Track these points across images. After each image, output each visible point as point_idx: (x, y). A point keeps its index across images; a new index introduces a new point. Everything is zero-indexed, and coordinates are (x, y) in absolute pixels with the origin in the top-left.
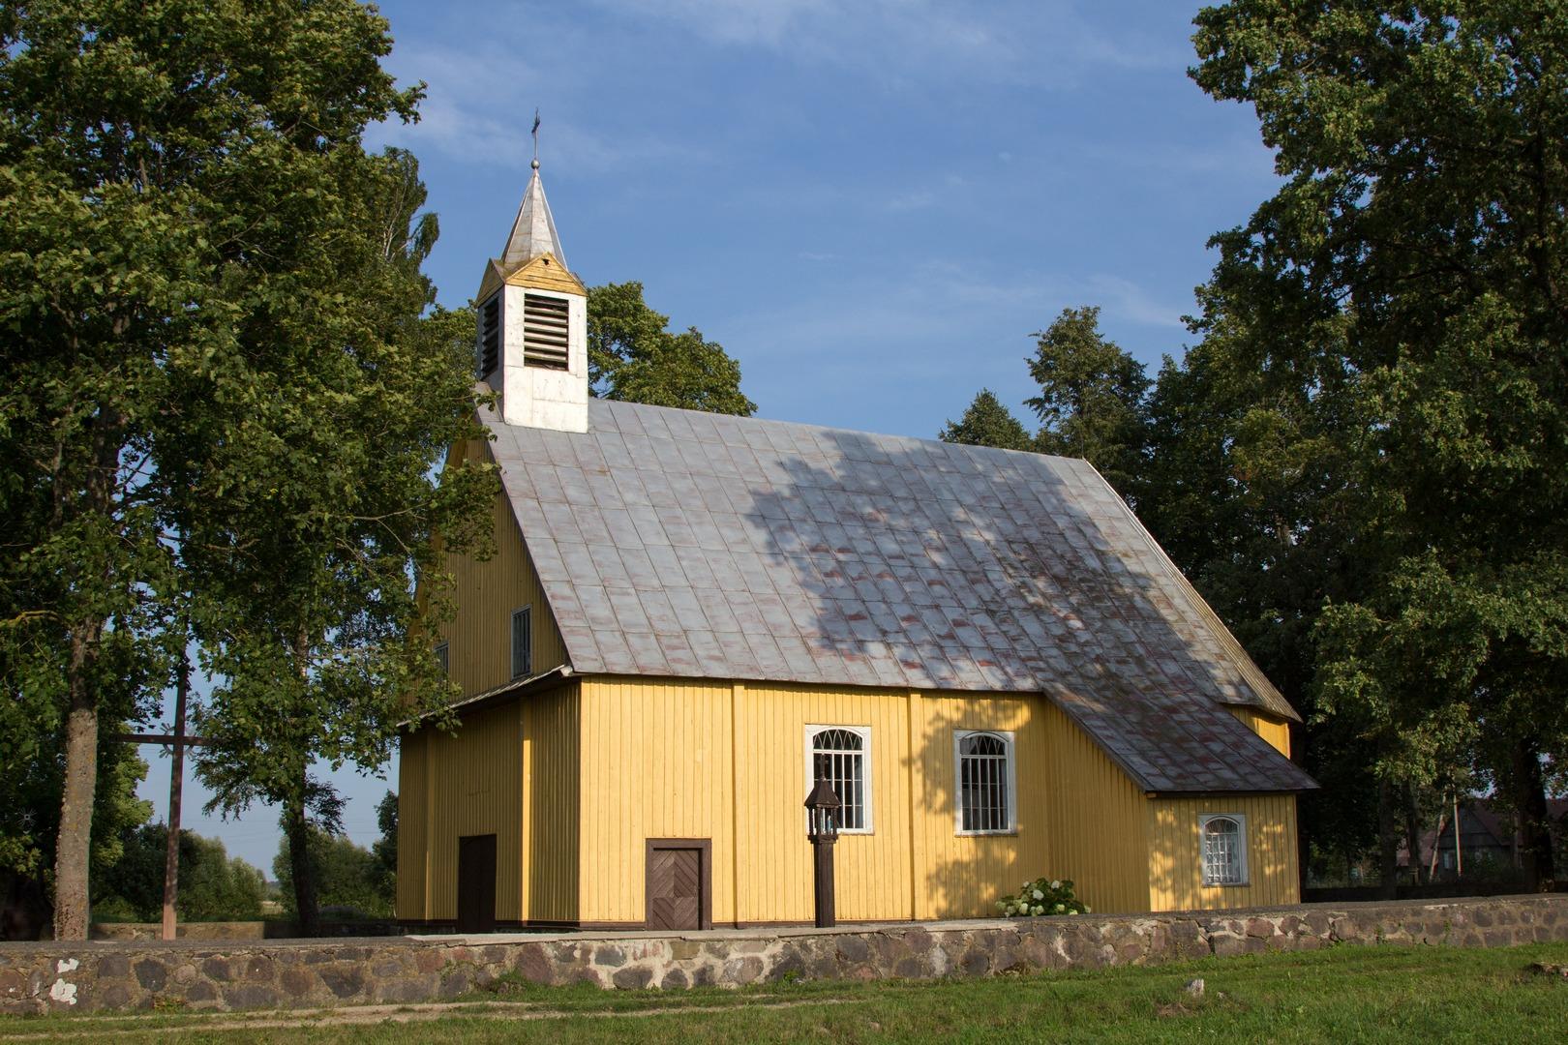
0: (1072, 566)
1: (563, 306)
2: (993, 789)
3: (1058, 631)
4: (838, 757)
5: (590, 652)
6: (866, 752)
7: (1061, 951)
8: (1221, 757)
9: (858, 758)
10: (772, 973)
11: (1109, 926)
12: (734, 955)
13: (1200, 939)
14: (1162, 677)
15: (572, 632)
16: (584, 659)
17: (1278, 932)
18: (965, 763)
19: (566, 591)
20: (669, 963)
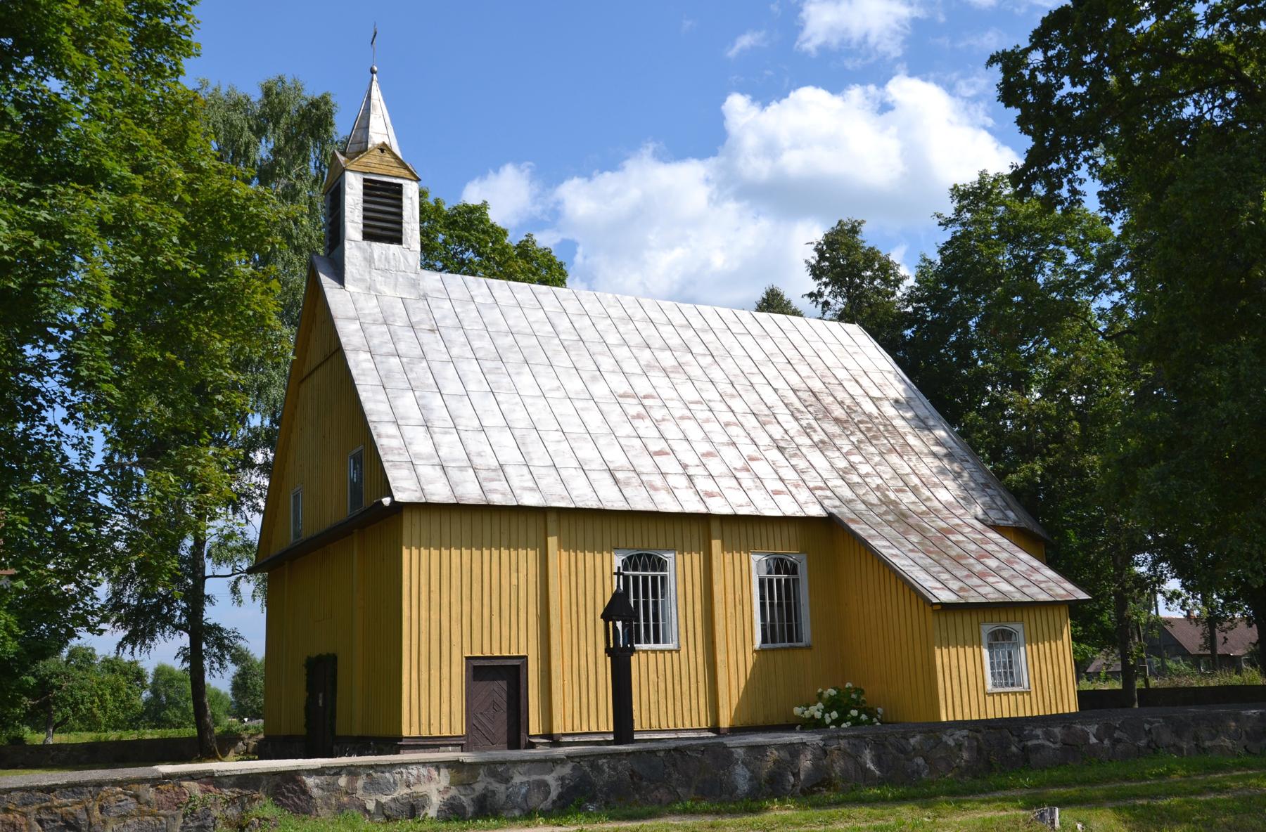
0: (850, 411)
1: (398, 190)
2: (788, 605)
3: (842, 464)
4: (645, 579)
5: (411, 484)
6: (670, 573)
7: (871, 766)
8: (996, 572)
9: (663, 578)
10: (560, 796)
11: (918, 737)
12: (517, 779)
13: (1014, 749)
14: (936, 504)
15: (395, 465)
16: (404, 490)
17: (1093, 740)
18: (762, 582)
19: (392, 430)
20: (447, 789)
